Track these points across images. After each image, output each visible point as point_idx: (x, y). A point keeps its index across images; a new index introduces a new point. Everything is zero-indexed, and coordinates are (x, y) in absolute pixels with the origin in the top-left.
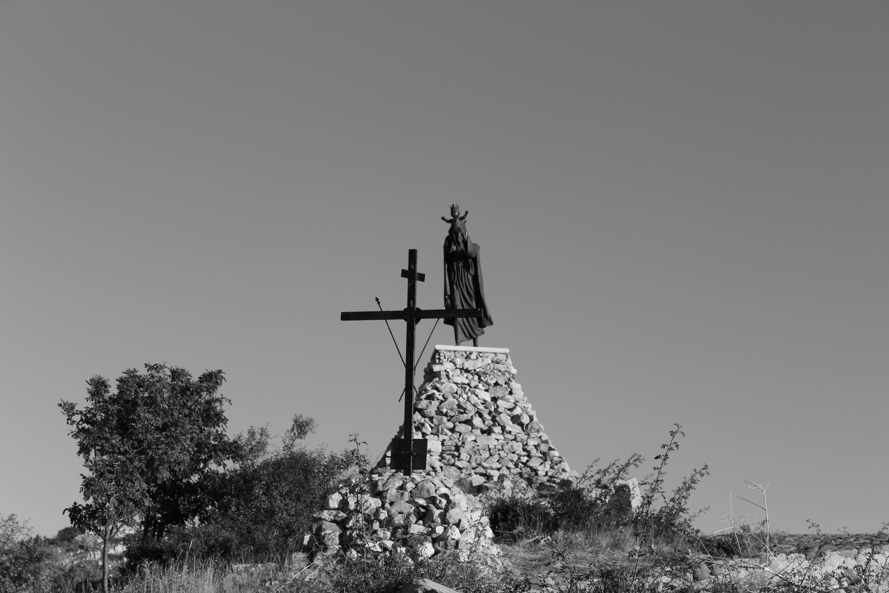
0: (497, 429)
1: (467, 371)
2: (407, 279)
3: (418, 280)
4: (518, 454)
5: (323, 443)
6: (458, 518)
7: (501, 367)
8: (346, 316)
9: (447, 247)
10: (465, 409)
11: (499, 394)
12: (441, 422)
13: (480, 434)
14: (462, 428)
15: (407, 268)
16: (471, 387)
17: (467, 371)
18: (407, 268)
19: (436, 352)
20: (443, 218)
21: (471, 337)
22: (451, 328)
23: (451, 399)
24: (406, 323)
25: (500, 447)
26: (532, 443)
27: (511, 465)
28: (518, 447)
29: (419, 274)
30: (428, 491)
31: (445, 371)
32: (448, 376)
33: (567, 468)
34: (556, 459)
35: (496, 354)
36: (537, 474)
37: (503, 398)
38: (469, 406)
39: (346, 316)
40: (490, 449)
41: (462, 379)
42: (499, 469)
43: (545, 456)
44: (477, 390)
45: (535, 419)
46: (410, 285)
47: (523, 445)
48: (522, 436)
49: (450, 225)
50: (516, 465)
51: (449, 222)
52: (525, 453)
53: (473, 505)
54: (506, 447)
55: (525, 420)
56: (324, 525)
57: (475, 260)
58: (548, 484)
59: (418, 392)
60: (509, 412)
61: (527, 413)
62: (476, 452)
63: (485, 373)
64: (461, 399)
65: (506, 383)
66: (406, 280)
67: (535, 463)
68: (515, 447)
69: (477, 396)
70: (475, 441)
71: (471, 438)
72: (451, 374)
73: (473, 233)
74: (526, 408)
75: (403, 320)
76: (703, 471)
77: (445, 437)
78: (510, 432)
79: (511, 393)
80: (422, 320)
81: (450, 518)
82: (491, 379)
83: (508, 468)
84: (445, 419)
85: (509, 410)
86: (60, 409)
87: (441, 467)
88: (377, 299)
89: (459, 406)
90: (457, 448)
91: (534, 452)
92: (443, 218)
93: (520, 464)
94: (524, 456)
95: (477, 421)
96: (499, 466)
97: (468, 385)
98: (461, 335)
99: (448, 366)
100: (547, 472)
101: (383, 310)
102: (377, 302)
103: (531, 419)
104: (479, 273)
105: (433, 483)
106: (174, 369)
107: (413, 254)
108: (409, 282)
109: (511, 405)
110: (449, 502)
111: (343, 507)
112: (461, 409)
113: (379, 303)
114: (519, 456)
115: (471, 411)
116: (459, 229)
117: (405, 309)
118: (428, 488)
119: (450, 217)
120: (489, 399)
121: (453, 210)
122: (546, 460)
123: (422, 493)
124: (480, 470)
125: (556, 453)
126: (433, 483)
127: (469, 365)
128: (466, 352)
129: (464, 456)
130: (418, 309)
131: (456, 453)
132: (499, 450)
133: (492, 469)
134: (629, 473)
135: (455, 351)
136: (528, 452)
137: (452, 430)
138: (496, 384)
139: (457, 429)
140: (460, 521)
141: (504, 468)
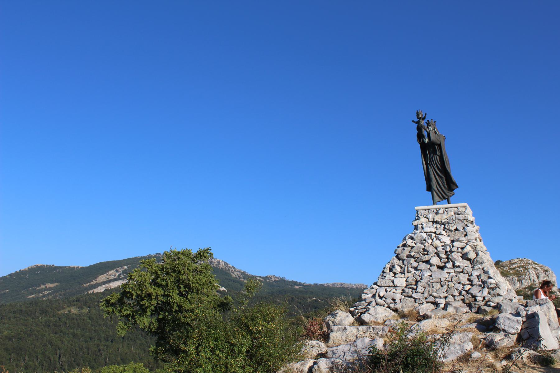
1: (437, 222)
14: (422, 266)
17: (437, 222)
19: (417, 211)
20: (413, 121)
27: (456, 293)
32: (422, 228)
35: (457, 208)
36: (476, 300)
38: (431, 249)
44: (440, 236)
49: (417, 125)
52: (469, 282)
54: (455, 279)
55: (472, 255)
62: (430, 284)
64: (426, 244)
67: (475, 291)
68: (461, 278)
69: (440, 240)
70: (431, 276)
72: (424, 226)
77: (410, 275)
78: (459, 267)
82: (452, 227)
89: (424, 250)
91: (476, 281)
92: (413, 121)
95: (435, 261)
98: (437, 198)
99: (423, 220)
112: (426, 252)
114: (464, 285)
119: (416, 120)
121: (418, 114)
122: (484, 288)
127: (437, 218)
128: (436, 209)
129: (420, 289)
131: (415, 287)
133: (440, 298)
135: (428, 210)
137: (416, 269)
138: (456, 230)
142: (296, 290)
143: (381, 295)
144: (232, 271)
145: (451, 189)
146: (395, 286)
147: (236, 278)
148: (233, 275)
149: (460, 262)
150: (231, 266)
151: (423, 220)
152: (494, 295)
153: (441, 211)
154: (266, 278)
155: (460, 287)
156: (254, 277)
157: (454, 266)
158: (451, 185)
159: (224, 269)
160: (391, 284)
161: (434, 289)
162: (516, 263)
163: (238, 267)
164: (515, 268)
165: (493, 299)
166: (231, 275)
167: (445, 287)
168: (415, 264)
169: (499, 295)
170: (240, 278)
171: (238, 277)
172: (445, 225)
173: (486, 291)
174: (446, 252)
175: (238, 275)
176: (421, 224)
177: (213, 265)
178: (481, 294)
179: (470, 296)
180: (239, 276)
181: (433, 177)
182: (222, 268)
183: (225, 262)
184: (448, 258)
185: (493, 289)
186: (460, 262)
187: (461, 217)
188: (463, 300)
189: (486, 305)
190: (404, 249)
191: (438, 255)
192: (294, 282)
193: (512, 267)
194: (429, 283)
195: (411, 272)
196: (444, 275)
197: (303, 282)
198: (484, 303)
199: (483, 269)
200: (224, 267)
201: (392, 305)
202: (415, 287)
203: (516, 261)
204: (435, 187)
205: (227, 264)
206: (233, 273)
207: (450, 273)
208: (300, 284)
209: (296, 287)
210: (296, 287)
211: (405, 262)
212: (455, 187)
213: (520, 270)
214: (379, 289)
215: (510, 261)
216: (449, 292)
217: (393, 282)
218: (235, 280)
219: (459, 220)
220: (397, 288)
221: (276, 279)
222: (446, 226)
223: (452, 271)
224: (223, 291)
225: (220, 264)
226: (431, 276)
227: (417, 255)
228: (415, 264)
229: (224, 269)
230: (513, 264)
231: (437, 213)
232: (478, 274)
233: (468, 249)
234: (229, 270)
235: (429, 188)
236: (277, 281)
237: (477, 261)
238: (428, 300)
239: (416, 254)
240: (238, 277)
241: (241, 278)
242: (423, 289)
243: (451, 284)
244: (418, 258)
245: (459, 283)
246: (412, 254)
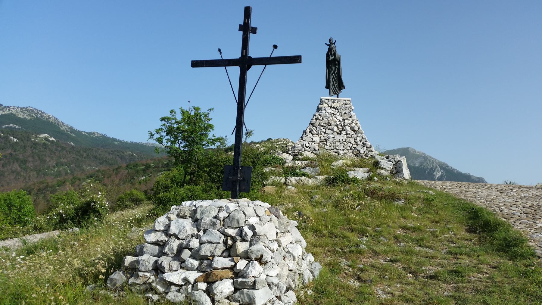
0: (344, 133)
1: (333, 108)
3: (251, 33)
4: (352, 144)
6: (260, 253)
7: (348, 106)
8: (196, 64)
9: (328, 55)
10: (331, 124)
11: (346, 118)
12: (320, 129)
13: (337, 134)
14: (328, 131)
15: (242, 24)
16: (334, 114)
17: (333, 108)
18: (242, 24)
19: (321, 100)
20: (326, 44)
21: (336, 94)
22: (328, 90)
23: (325, 119)
25: (345, 140)
26: (358, 139)
27: (349, 148)
28: (352, 140)
29: (252, 28)
30: (238, 222)
31: (324, 108)
32: (325, 110)
33: (374, 150)
34: (369, 146)
35: (345, 100)
36: (360, 153)
37: (347, 119)
38: (333, 123)
39: (196, 64)
40: (340, 141)
41: (331, 111)
42: (343, 150)
43: (364, 145)
44: (337, 116)
45: (360, 128)
46: (244, 36)
47: (355, 140)
48: (355, 135)
49: (328, 46)
50: (351, 149)
51: (328, 45)
52: (355, 143)
53: (285, 228)
54: (347, 140)
55: (356, 129)
56: (145, 248)
57: (339, 62)
58: (365, 157)
60: (349, 125)
61: (357, 126)
62: (334, 142)
63: (340, 109)
64: (329, 119)
65: (349, 113)
66: (241, 33)
67: (359, 148)
68: (351, 140)
69: (336, 118)
70: (334, 138)
71: (332, 136)
72: (326, 109)
73: (339, 51)
74: (359, 124)
75: (238, 67)
77: (322, 136)
78: (349, 134)
79: (351, 117)
80: (253, 67)
81: (252, 253)
82: (343, 111)
83: (347, 150)
84: (322, 128)
85: (349, 124)
86: (211, 118)
87: (319, 149)
88: (219, 50)
89: (328, 122)
90: (326, 140)
91: (359, 143)
92: (326, 44)
93: (353, 148)
94: (355, 144)
95: (335, 129)
96: (344, 149)
97: (333, 113)
98: (332, 94)
99: (325, 105)
100: (364, 152)
101: (223, 59)
103: (359, 128)
104: (340, 67)
105: (244, 213)
107: (248, 11)
108: (243, 34)
109: (350, 122)
110: (255, 234)
112: (329, 124)
113: (221, 53)
114: (353, 144)
115: (333, 125)
116: (332, 48)
117: (240, 58)
118: (238, 219)
119: (329, 43)
120: (341, 120)
121: (330, 40)
122: (364, 146)
123: (233, 223)
124: (335, 150)
125: (369, 144)
126: (244, 213)
127: (334, 105)
128: (333, 100)
129: (328, 144)
130: (250, 57)
131: (326, 143)
132: (344, 142)
133: (340, 150)
135: (328, 100)
136: (357, 143)
137: (325, 133)
138: (345, 113)
139: (326, 132)
140: (262, 256)
141: (346, 149)
142: (115, 145)
143: (307, 146)
144: (61, 125)
145: (340, 89)
146: (313, 142)
147: (64, 131)
148: (62, 129)
149: (349, 131)
150: (60, 121)
151: (325, 105)
152: (369, 151)
153: (336, 101)
154: (91, 133)
155: (351, 145)
156: (80, 132)
157: (347, 134)
158: (341, 86)
159: (54, 123)
160: (311, 140)
161: (337, 145)
162: (281, 141)
163: (66, 122)
164: (280, 145)
165: (369, 153)
166: (60, 129)
167: (343, 144)
168: (324, 130)
169: (372, 151)
170: (67, 131)
171: (65, 130)
172: (338, 110)
173: (365, 148)
174: (341, 125)
175: (65, 129)
176: (324, 108)
177: (44, 118)
178: (363, 150)
179: (356, 150)
180: (67, 130)
181: (331, 80)
182: (51, 122)
183: (55, 117)
184: (343, 129)
185: (369, 148)
186: (349, 131)
187: (348, 106)
188: (352, 152)
189: (365, 155)
190: (317, 121)
191: (337, 126)
192: (113, 138)
193: (278, 143)
194: (334, 141)
195: (322, 134)
196: (341, 138)
197: (121, 139)
198: (364, 154)
199: (362, 137)
200: (54, 121)
201: (314, 152)
202: (326, 143)
203: (281, 140)
204: (331, 87)
205: (57, 119)
206: (62, 127)
207: (344, 137)
208: (119, 141)
209: (116, 143)
210: (116, 143)
211: (318, 128)
212: (343, 88)
213: (283, 146)
214: (305, 143)
215: (277, 139)
216: (345, 147)
217: (312, 139)
218: (63, 133)
219: (347, 108)
220: (315, 143)
221: (99, 135)
222: (339, 111)
223: (345, 136)
224: (53, 141)
225: (50, 118)
226: (334, 138)
227: (325, 125)
228: (324, 130)
229: (54, 123)
230: (279, 141)
231: (334, 102)
232: (360, 139)
233: (353, 125)
234: (58, 124)
235: (328, 87)
236: (100, 137)
237: (359, 132)
238: (334, 151)
239: (324, 124)
240: (65, 130)
241: (68, 131)
242: (331, 144)
243: (345, 143)
244: (325, 127)
245: (350, 143)
246: (322, 124)
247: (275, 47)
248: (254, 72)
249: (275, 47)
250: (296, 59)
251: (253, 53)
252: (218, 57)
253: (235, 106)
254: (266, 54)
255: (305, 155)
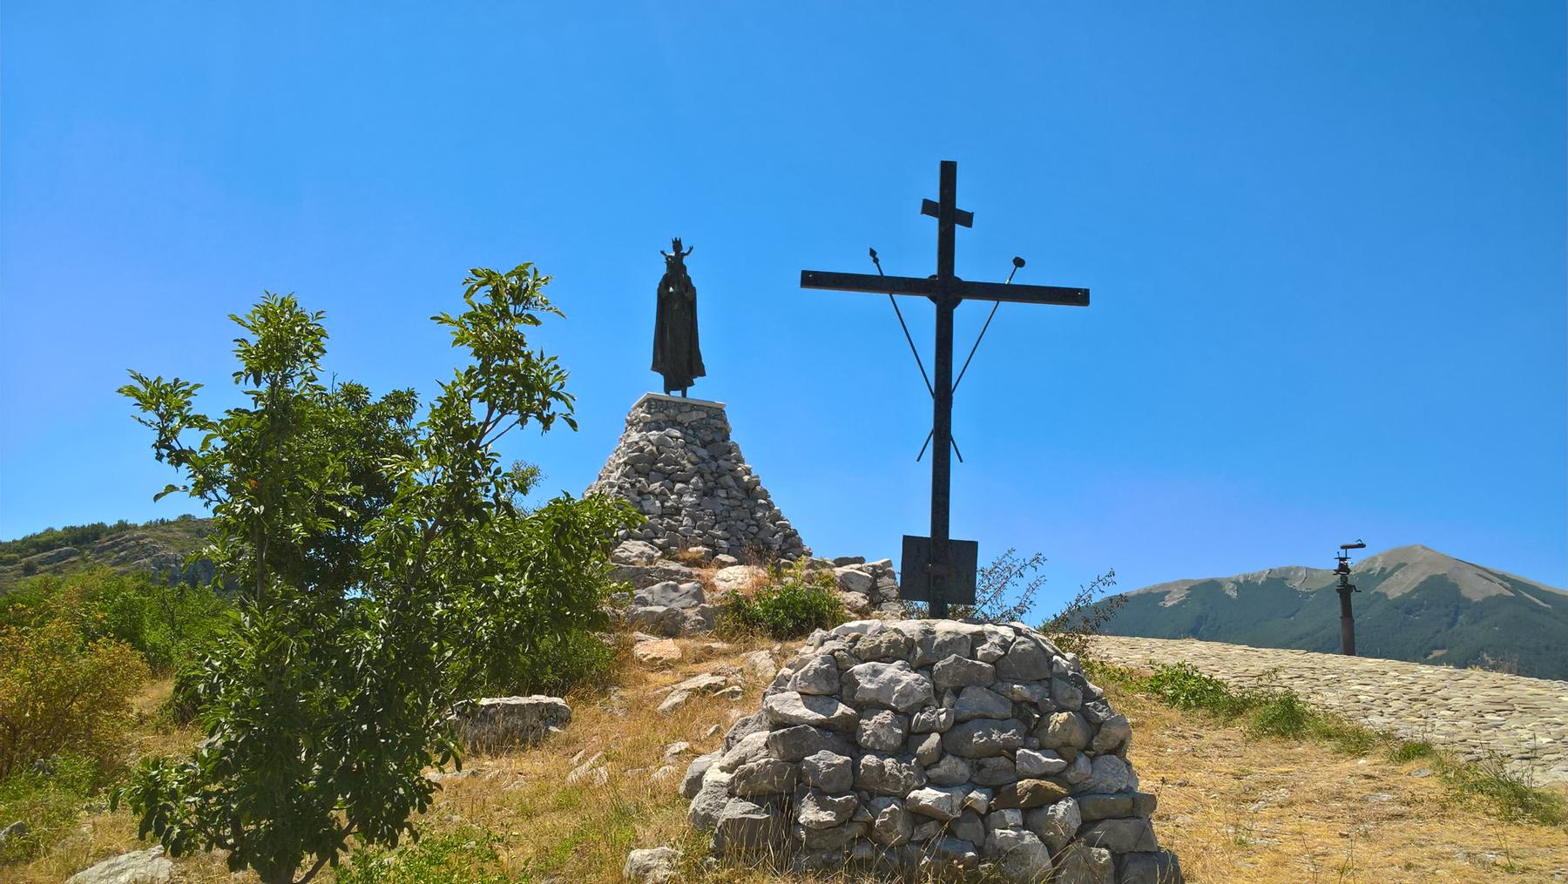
2: (957, 207)
5: (1087, 621)
8: (812, 279)
24: (662, 376)
39: (812, 279)
59: (952, 445)
76: (1109, 579)
88: (873, 253)
94: (753, 525)
101: (885, 274)
102: (872, 258)
106: (440, 399)
107: (948, 172)
108: (941, 224)
111: (841, 690)
113: (876, 261)
134: (530, 461)
170: (650, 559)
207: (723, 505)
247: (1019, 262)
248: (922, 310)
249: (1019, 262)
250: (1077, 297)
251: (927, 268)
252: (871, 270)
253: (929, 405)
254: (1001, 275)
255: (721, 585)
